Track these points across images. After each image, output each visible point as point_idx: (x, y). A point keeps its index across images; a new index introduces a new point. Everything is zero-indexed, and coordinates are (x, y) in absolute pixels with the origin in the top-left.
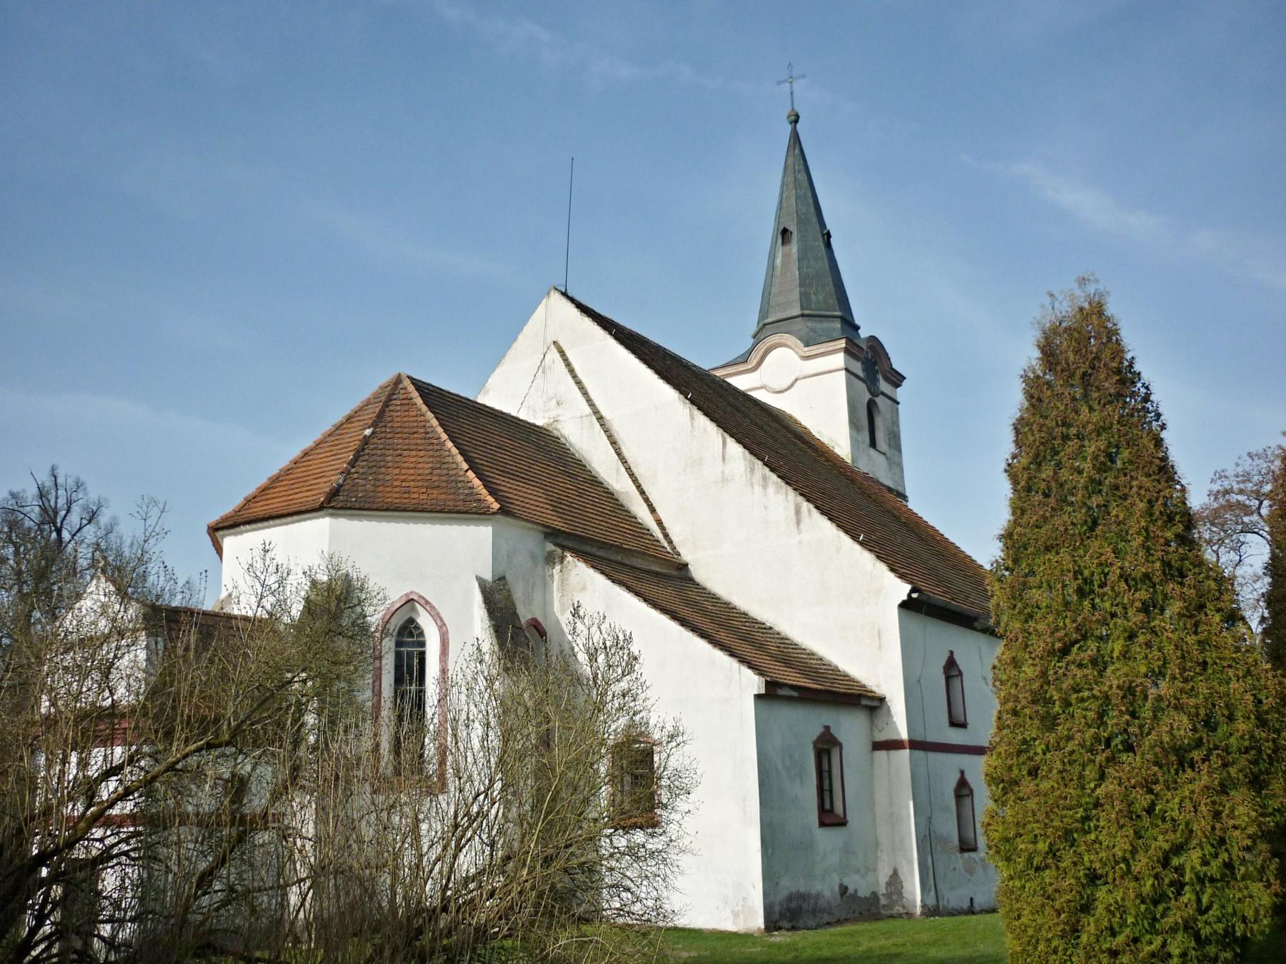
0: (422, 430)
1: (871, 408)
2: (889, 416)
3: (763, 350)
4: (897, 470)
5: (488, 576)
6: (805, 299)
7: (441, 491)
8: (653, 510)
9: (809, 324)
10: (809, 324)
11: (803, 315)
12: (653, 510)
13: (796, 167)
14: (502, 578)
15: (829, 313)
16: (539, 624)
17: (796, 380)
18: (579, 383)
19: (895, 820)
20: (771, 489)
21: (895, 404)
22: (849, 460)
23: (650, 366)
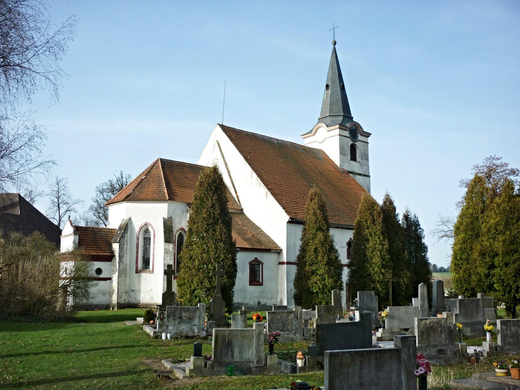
0: (158, 176)
1: (353, 148)
2: (362, 148)
3: (316, 129)
4: (365, 167)
5: (166, 217)
6: (331, 109)
7: (156, 194)
8: (236, 193)
9: (331, 119)
10: (331, 119)
11: (329, 116)
12: (236, 193)
13: (333, 61)
14: (171, 218)
15: (338, 114)
16: (184, 229)
17: (325, 139)
18: (222, 154)
19: (282, 284)
20: (261, 187)
21: (367, 144)
22: (339, 166)
23: (238, 149)
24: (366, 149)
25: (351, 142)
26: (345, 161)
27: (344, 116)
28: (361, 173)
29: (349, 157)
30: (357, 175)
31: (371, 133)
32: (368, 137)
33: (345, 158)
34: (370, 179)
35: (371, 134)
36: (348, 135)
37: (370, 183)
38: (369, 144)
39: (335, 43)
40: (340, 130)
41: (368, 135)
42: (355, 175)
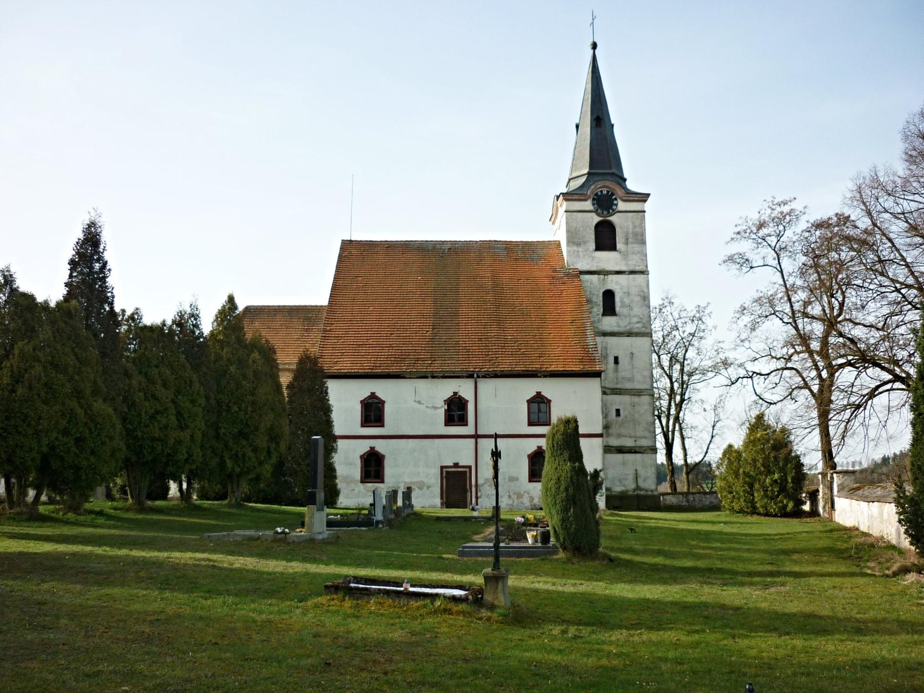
24: (637, 224)
25: (597, 219)
26: (581, 255)
27: (589, 173)
28: (623, 268)
29: (592, 245)
30: (611, 274)
31: (78, 234)
32: (645, 201)
33: (580, 249)
34: (648, 278)
35: (648, 195)
36: (591, 208)
37: (648, 285)
38: (646, 214)
39: (594, 46)
40: (568, 202)
41: (643, 198)
42: (605, 275)
